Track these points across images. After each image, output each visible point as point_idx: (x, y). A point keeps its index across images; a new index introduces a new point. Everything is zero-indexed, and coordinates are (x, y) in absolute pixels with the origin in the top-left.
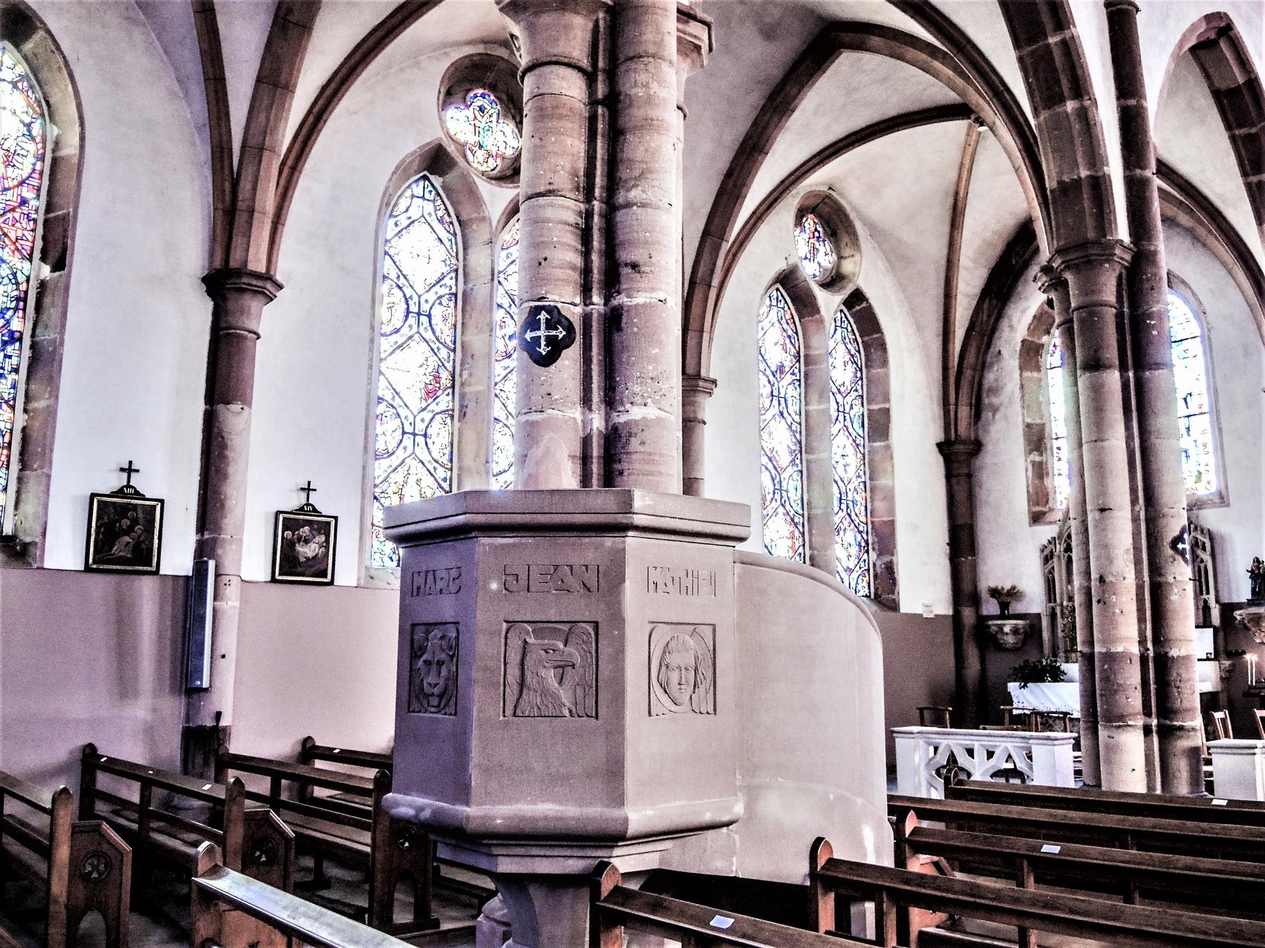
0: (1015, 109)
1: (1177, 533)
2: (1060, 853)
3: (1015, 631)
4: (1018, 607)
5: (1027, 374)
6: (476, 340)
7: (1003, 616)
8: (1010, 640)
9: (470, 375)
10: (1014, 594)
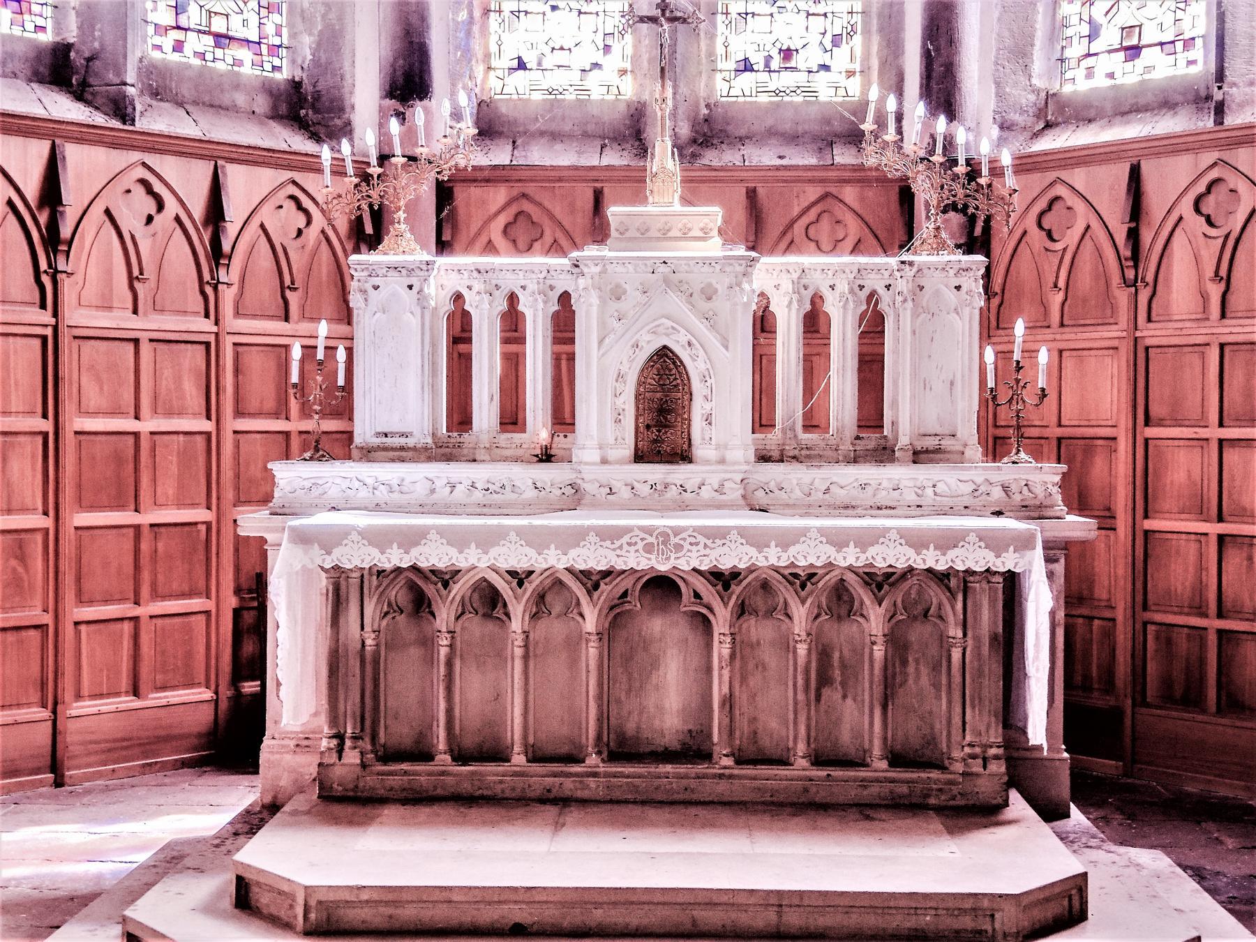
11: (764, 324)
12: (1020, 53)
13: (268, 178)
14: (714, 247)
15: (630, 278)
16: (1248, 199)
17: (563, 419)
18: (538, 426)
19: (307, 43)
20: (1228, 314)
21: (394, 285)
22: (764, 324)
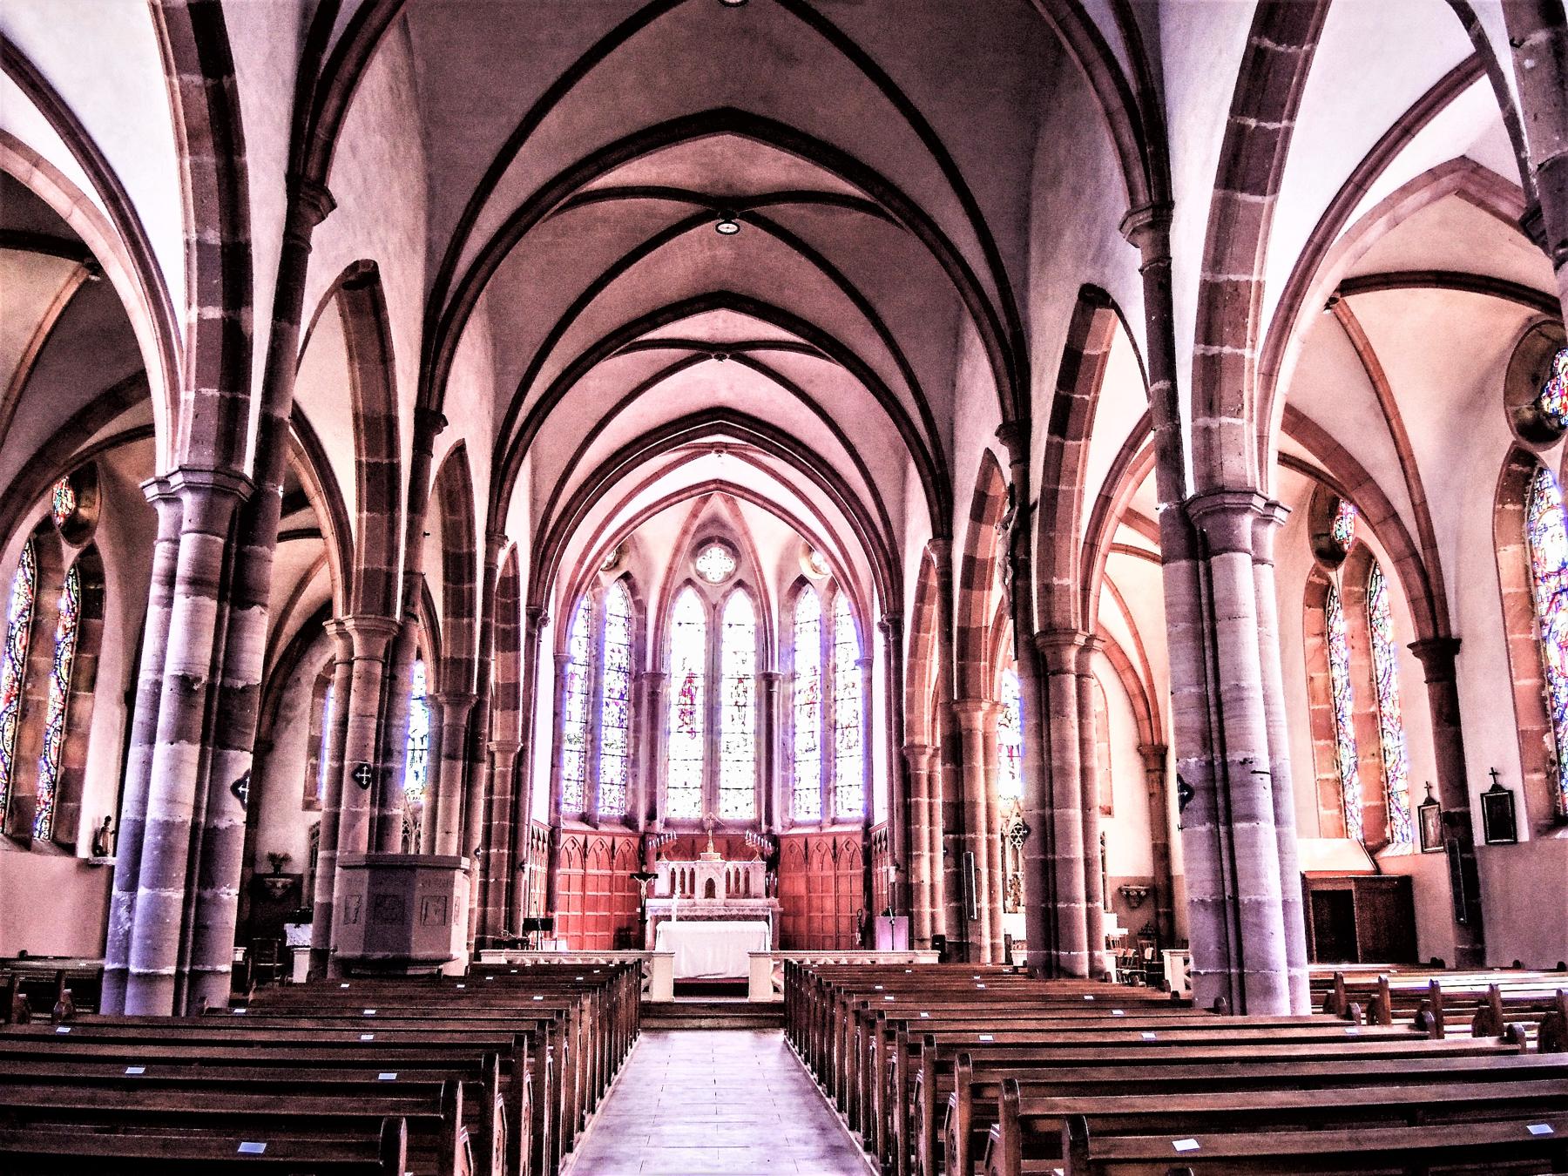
0: (152, 266)
1: (240, 777)
2: (146, 1072)
3: (284, 886)
4: (286, 869)
5: (317, 700)
6: (41, 661)
7: (274, 875)
8: (279, 893)
9: (34, 686)
10: (286, 859)
11: (728, 874)
12: (786, 810)
13: (623, 839)
14: (719, 860)
15: (704, 865)
16: (1563, 701)
17: (692, 890)
18: (687, 892)
19: (628, 809)
20: (1496, 937)
21: (662, 867)
22: (728, 874)
